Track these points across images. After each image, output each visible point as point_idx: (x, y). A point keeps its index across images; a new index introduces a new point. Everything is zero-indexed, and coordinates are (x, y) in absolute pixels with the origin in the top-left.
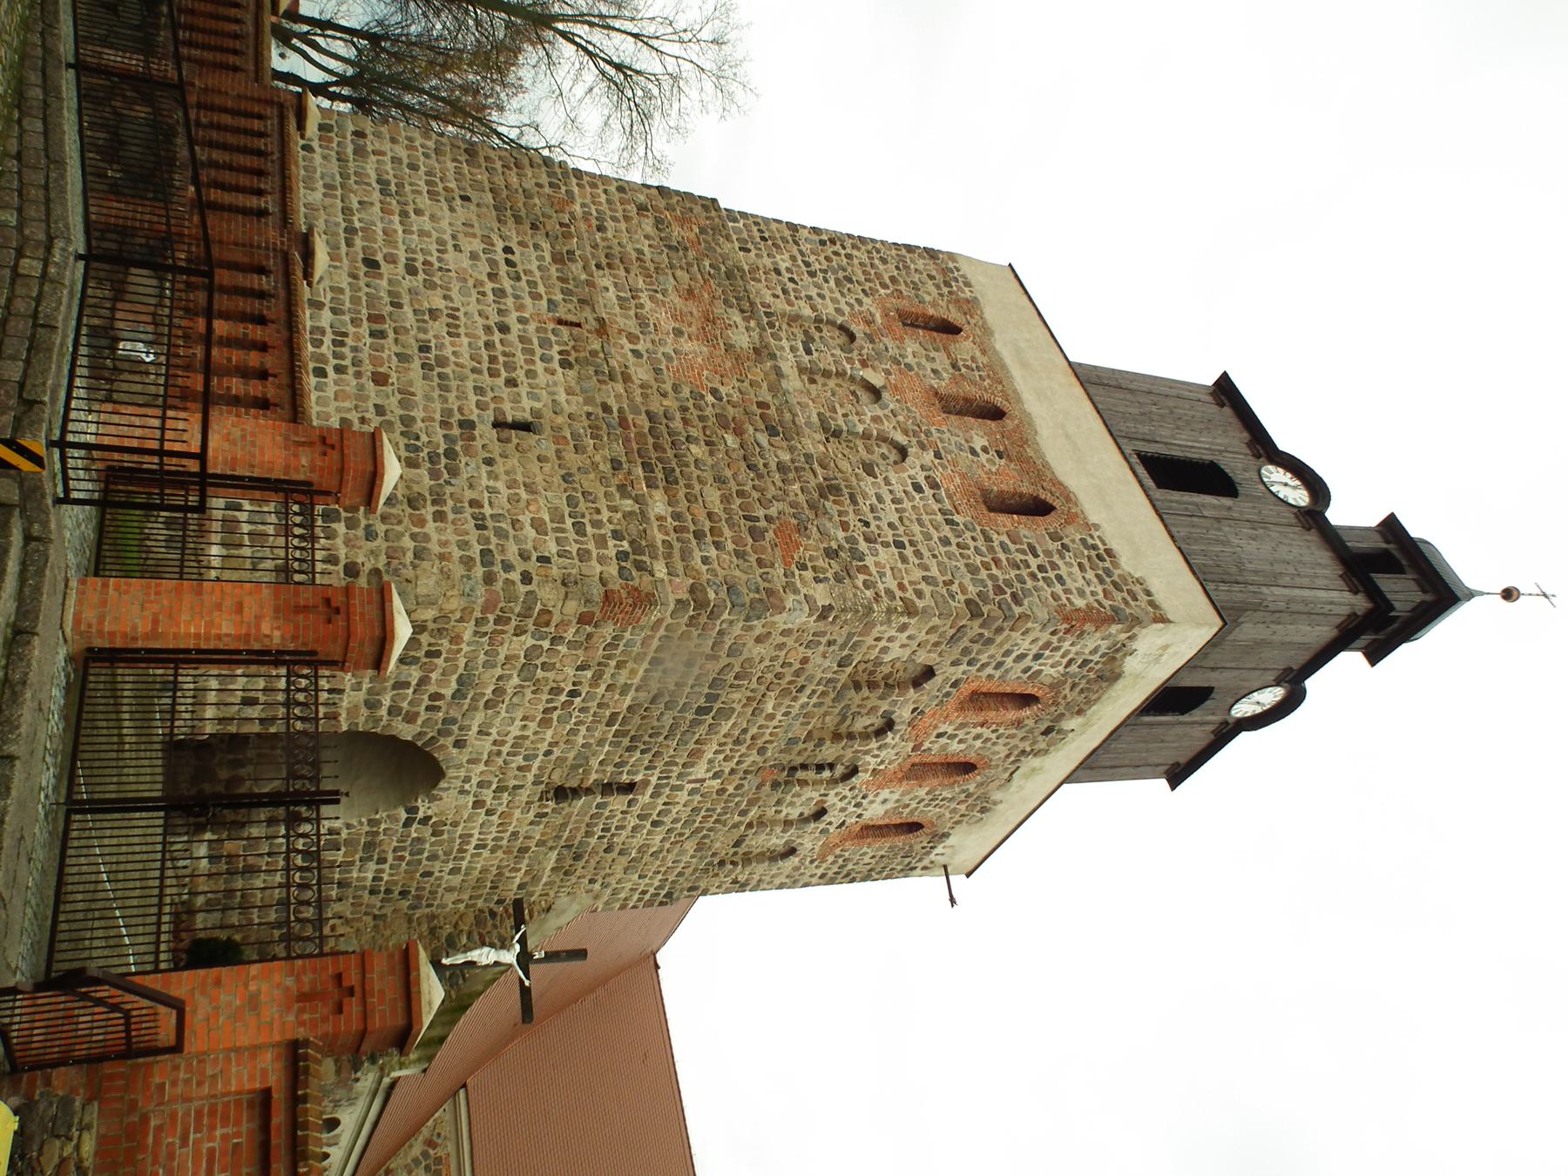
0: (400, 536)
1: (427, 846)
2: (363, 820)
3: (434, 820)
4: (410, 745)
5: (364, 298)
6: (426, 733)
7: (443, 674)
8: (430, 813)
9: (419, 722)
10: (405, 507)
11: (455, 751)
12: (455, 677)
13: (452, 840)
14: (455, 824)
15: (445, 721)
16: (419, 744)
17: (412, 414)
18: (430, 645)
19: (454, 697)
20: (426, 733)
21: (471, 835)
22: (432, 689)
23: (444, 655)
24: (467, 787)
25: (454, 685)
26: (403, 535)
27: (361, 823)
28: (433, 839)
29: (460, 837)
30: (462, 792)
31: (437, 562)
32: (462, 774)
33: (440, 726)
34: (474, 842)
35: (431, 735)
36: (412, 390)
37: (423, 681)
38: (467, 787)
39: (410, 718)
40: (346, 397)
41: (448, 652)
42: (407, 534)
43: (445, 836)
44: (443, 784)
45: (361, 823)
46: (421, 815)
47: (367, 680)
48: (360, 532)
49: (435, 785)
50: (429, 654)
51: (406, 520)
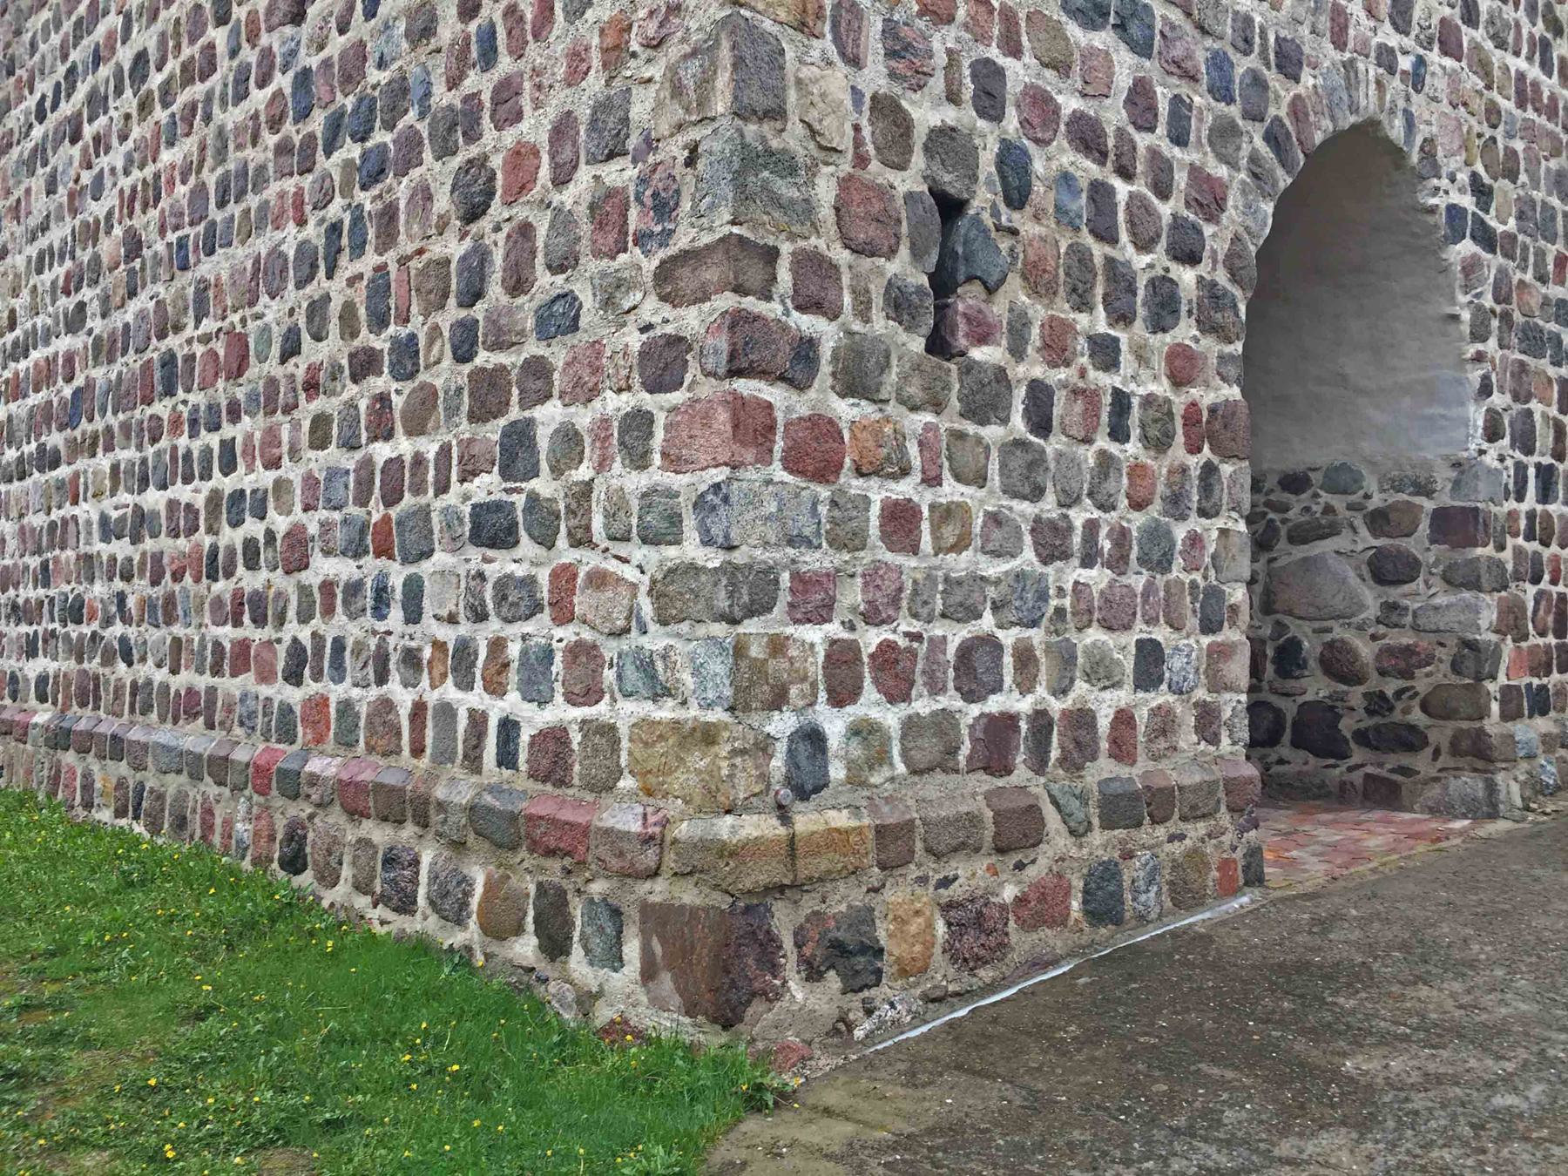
0: (563, 220)
1: (1538, 195)
2: (1471, 350)
3: (1479, 168)
4: (1287, 205)
5: (121, 416)
6: (1254, 159)
7: (1061, 67)
8: (1464, 177)
9: (1222, 171)
10: (485, 224)
11: (1308, 79)
12: (1074, 31)
13: (1529, 130)
14: (1493, 114)
15: (1222, 93)
16: (1284, 180)
17: (291, 254)
18: (953, 98)
19: (1142, 48)
20: (1254, 159)
21: (1521, 76)
22: (1113, 115)
23: (994, 53)
24: (1405, 63)
25: (1103, 39)
26: (558, 211)
27: (1479, 358)
28: (1523, 178)
29: (1521, 105)
30: (1417, 79)
31: (632, 68)
32: (1369, 69)
33: (1234, 111)
34: (1534, 72)
35: (1259, 142)
36: (249, 264)
37: (1087, 137)
38: (1405, 63)
39: (1209, 200)
40: (272, 437)
41: (982, 38)
42: (556, 198)
43: (1519, 145)
44: (1396, 130)
45: (1479, 358)
46: (1467, 202)
47: (1082, 320)
48: (557, 354)
49: (1397, 154)
50: (990, 102)
51: (521, 212)
